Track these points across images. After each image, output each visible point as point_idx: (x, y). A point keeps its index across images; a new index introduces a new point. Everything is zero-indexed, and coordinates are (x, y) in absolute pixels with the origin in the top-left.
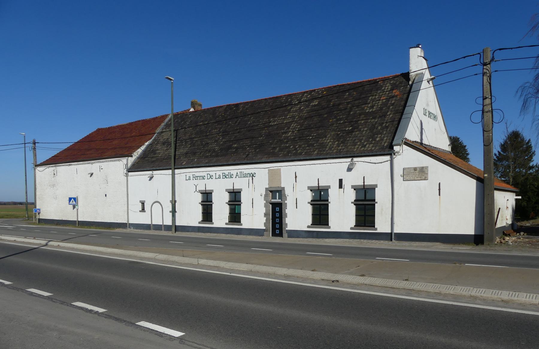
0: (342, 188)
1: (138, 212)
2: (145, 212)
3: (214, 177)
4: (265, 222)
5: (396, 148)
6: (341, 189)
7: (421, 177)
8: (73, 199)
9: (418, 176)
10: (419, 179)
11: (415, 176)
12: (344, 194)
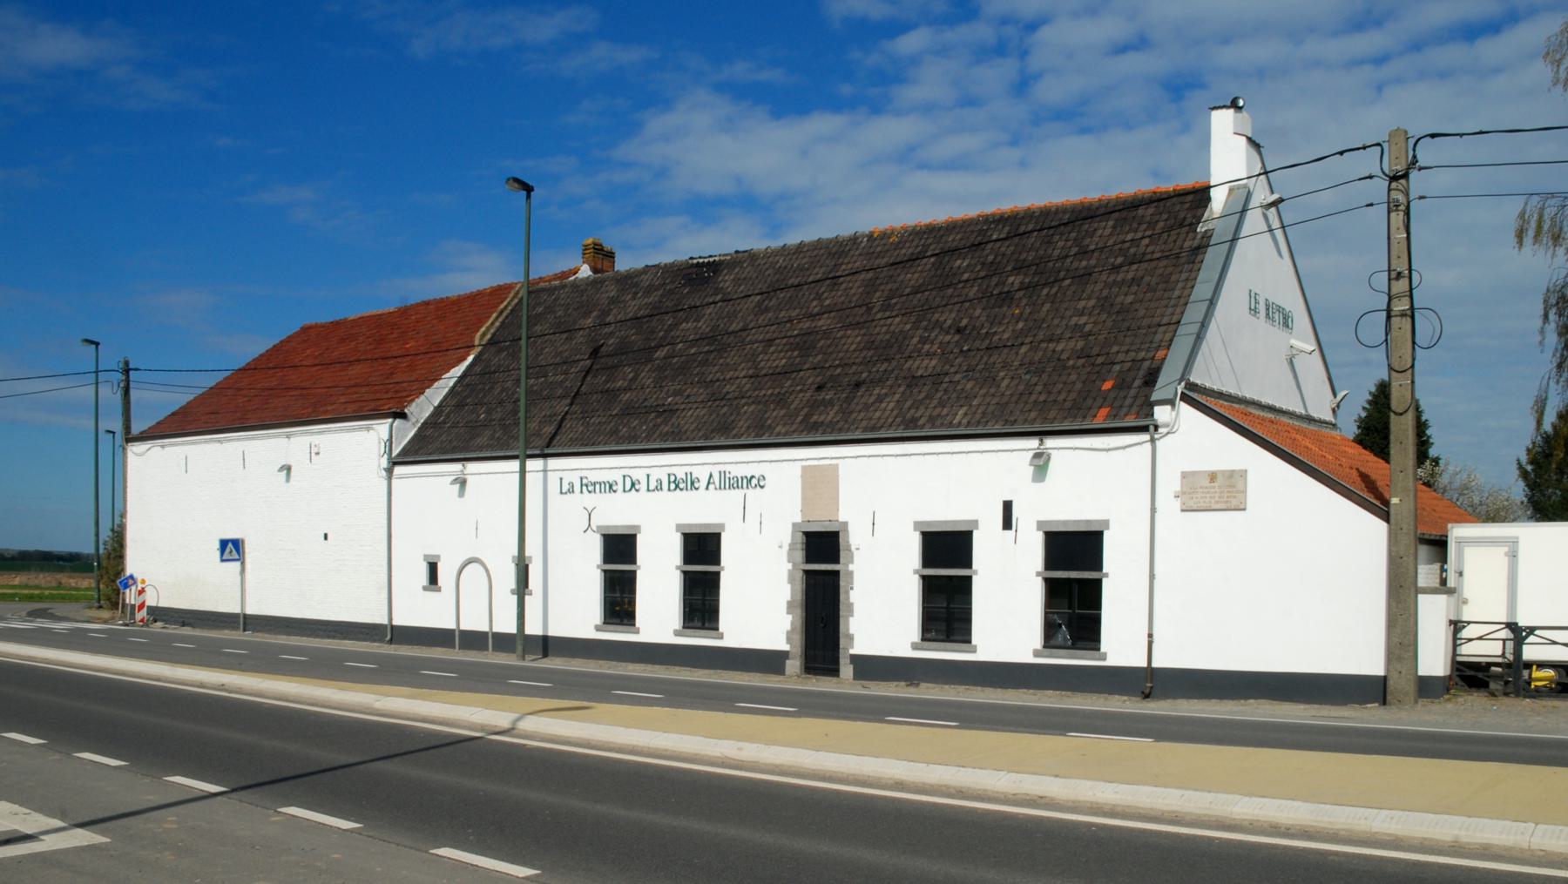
2: (439, 590)
3: (643, 486)
8: (230, 545)
9: (1220, 497)
10: (1224, 506)
11: (1211, 497)
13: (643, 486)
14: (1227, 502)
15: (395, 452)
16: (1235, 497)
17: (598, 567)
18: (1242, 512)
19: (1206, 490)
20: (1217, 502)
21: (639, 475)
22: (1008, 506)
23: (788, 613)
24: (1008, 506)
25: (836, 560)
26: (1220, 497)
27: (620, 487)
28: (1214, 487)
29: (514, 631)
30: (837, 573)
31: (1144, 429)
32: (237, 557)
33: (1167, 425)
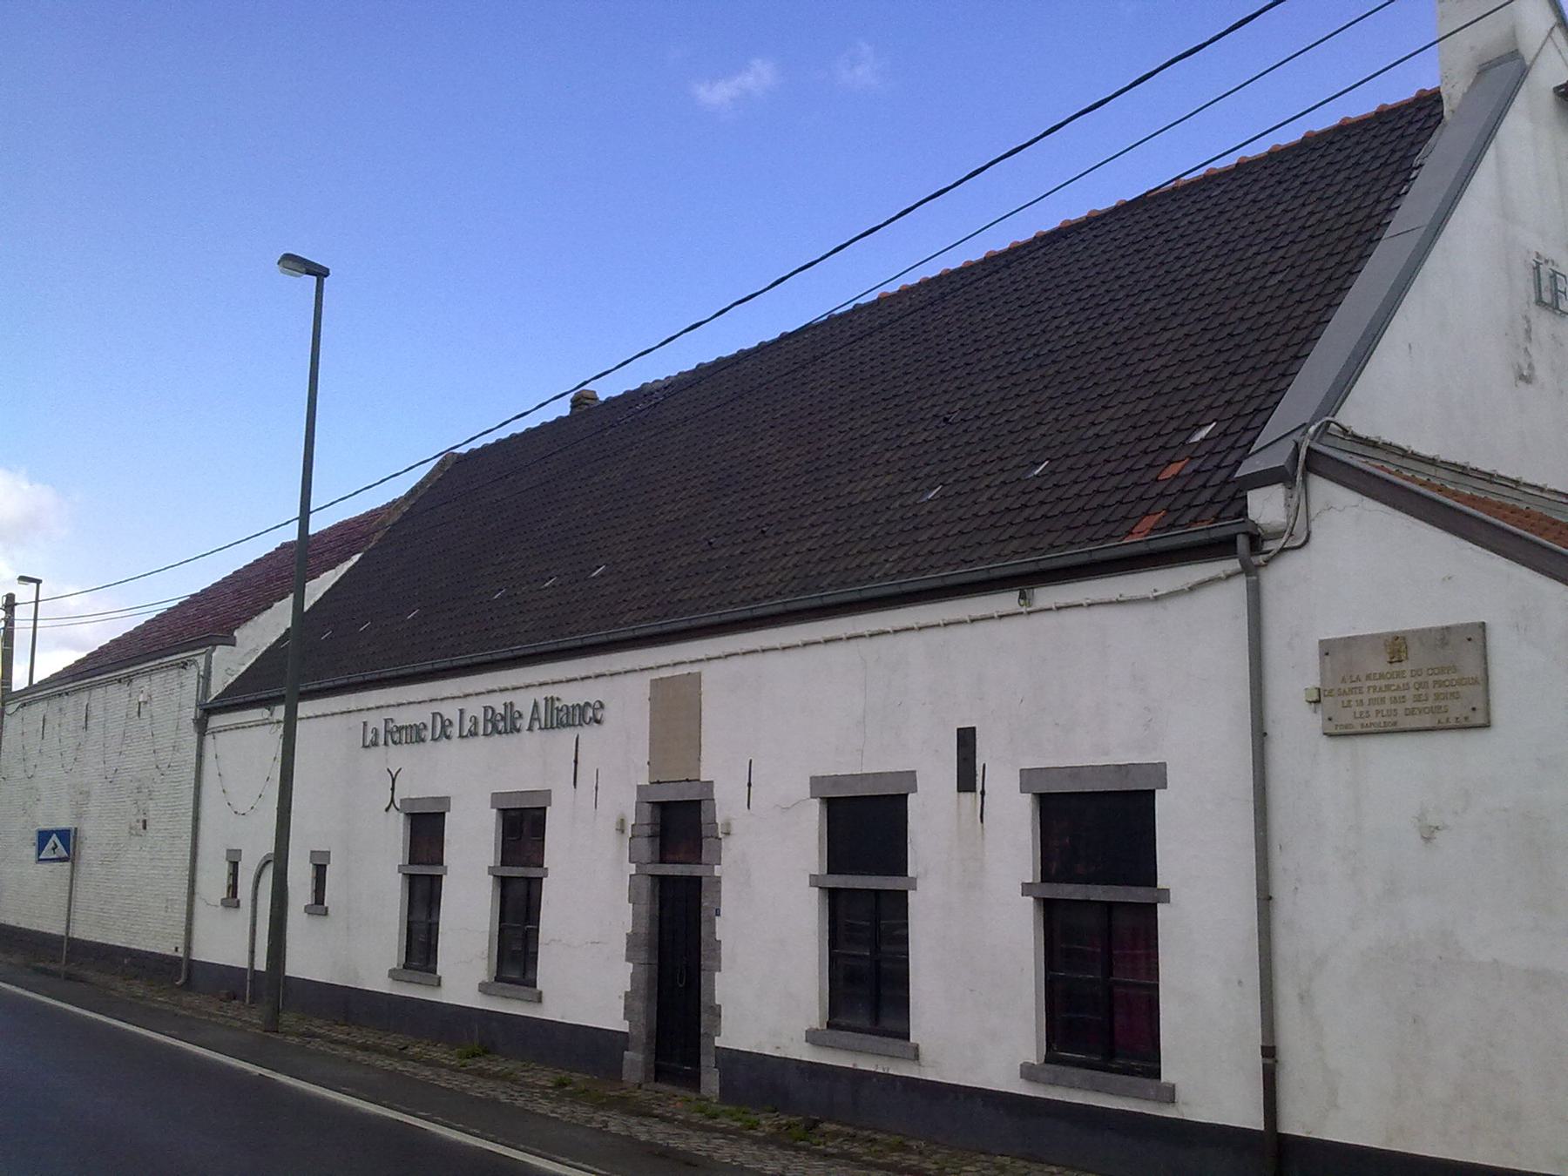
0: (974, 790)
1: (216, 906)
2: (326, 913)
3: (455, 731)
4: (629, 990)
5: (1266, 507)
6: (969, 795)
7: (1434, 710)
8: (54, 837)
9: (1418, 699)
10: (1427, 720)
11: (1394, 700)
12: (982, 827)
13: (455, 731)
14: (1434, 710)
15: (217, 688)
16: (1456, 696)
17: (491, 870)
18: (1474, 736)
19: (1383, 683)
20: (1410, 712)
21: (450, 711)
22: (966, 739)
23: (628, 959)
24: (966, 739)
25: (695, 855)
26: (1418, 699)
27: (428, 734)
28: (1400, 675)
29: (1259, 1125)
30: (697, 881)
31: (1219, 548)
32: (65, 854)
33: (1277, 535)
